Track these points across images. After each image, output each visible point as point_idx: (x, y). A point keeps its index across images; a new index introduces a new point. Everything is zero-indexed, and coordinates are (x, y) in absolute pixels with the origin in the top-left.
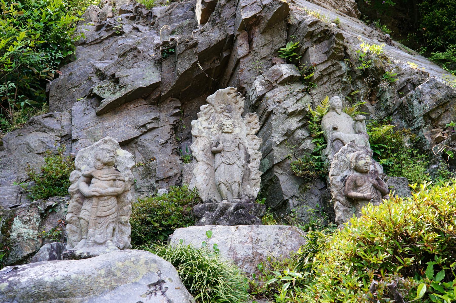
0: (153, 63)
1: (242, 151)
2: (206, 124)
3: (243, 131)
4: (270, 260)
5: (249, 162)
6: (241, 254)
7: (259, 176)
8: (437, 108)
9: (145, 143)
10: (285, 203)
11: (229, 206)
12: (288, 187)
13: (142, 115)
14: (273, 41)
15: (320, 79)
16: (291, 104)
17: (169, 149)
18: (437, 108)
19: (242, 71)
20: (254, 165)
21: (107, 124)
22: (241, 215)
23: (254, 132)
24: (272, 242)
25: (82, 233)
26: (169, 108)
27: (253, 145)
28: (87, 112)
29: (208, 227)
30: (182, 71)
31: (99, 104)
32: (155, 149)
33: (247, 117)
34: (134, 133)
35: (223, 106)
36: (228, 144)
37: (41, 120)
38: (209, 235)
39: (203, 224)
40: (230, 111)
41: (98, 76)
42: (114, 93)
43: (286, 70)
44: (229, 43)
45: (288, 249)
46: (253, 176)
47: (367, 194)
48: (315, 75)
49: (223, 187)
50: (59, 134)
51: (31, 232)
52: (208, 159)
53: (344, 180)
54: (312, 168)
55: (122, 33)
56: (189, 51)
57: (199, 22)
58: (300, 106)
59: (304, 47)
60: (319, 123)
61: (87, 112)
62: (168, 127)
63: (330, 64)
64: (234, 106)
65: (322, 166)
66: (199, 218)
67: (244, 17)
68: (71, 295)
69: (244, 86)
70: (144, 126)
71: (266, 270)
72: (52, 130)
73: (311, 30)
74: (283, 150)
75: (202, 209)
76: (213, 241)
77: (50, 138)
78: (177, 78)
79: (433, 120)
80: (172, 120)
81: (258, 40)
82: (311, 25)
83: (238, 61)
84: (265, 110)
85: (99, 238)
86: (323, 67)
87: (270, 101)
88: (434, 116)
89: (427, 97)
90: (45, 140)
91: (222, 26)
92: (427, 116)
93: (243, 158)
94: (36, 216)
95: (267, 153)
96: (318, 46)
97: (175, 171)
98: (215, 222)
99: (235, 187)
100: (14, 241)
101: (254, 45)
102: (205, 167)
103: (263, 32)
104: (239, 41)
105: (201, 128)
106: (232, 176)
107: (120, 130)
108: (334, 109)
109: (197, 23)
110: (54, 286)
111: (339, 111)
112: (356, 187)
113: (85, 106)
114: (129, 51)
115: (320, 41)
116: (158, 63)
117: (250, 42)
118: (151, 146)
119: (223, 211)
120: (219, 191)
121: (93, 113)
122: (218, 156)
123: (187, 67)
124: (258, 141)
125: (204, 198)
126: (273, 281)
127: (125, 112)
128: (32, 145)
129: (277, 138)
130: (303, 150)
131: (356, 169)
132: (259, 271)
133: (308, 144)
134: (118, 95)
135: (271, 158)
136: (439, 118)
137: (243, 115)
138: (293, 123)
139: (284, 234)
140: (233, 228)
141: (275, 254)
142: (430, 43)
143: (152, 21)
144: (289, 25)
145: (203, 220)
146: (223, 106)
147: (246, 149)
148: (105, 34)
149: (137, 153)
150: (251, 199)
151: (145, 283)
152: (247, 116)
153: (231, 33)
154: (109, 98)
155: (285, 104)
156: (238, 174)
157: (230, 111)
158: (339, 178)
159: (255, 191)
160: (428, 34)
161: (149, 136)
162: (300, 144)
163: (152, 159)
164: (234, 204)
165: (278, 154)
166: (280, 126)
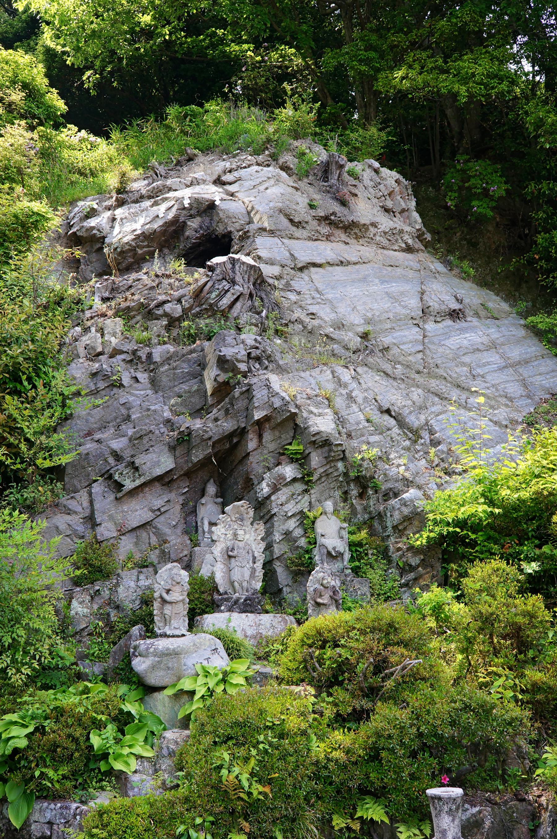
0: (167, 448)
1: (251, 555)
2: (223, 531)
3: (251, 537)
4: (267, 637)
5: (255, 563)
6: (249, 633)
7: (262, 574)
8: (404, 521)
9: (159, 526)
10: (280, 590)
11: (240, 598)
12: (283, 577)
13: (157, 499)
14: (280, 437)
15: (319, 479)
16: (291, 507)
17: (179, 531)
18: (404, 521)
19: (251, 463)
20: (259, 565)
21: (125, 508)
22: (248, 606)
23: (259, 538)
24: (268, 626)
25: (166, 621)
26: (179, 488)
27: (258, 549)
28: (105, 495)
29: (227, 614)
30: (195, 459)
31: (120, 491)
32: (167, 531)
33: (256, 526)
34: (149, 516)
35: (237, 516)
36: (241, 551)
37: (65, 503)
38: (229, 621)
39: (222, 611)
40: (242, 520)
41: (113, 456)
42: (134, 481)
43: (289, 471)
44: (241, 433)
45: (277, 631)
46: (257, 574)
47: (325, 602)
48: (314, 478)
49: (236, 584)
50: (81, 516)
51: (85, 610)
52: (225, 560)
53: (315, 590)
54: (302, 565)
55: (121, 386)
56: (204, 443)
57: (209, 393)
58: (299, 508)
59: (307, 452)
60: (313, 523)
61: (105, 495)
62: (178, 507)
63: (328, 467)
64: (245, 516)
65: (311, 563)
66: (218, 606)
67: (256, 418)
68: (181, 654)
69: (253, 477)
70: (159, 510)
71: (264, 643)
72: (76, 513)
73: (314, 439)
74: (282, 546)
75: (221, 600)
76: (232, 624)
77: (76, 521)
78: (190, 465)
79: (400, 530)
80: (181, 499)
81: (267, 436)
82: (314, 435)
83: (248, 454)
84: (269, 511)
85: (176, 625)
86: (322, 470)
87: (274, 505)
88: (401, 527)
89: (397, 513)
90: (71, 523)
91: (235, 416)
92: (395, 527)
93: (251, 562)
94: (88, 598)
95: (269, 548)
96: (319, 451)
97: (186, 552)
98: (230, 610)
99: (245, 584)
100: (73, 617)
101: (264, 440)
102: (222, 566)
103: (273, 429)
104: (251, 436)
105: (219, 533)
106: (243, 576)
107: (137, 513)
108: (326, 514)
109: (206, 392)
110: (174, 650)
111: (329, 516)
112: (321, 596)
113: (103, 488)
114: (145, 435)
115: (321, 447)
116: (172, 448)
117: (260, 437)
118: (164, 528)
119: (236, 602)
120: (233, 587)
121: (112, 497)
122: (233, 560)
123: (201, 457)
124: (263, 545)
125: (221, 590)
126: (267, 650)
127: (141, 495)
128: (60, 528)
129: (277, 537)
130: (298, 547)
131: (322, 585)
132: (259, 644)
133: (302, 542)
134: (138, 483)
135: (272, 553)
136: (405, 529)
137: (252, 524)
138: (292, 524)
139: (276, 620)
140: (244, 615)
141: (270, 633)
142: (542, 281)
143: (152, 367)
144: (296, 425)
145: (222, 608)
146: (237, 516)
147: (253, 552)
148: (102, 385)
149: (151, 534)
150: (255, 592)
151: (209, 649)
152: (255, 525)
153: (243, 425)
154: (129, 485)
155: (286, 508)
156: (247, 574)
157: (242, 520)
158: (312, 589)
159: (258, 585)
160: (542, 267)
161: (162, 518)
162: (296, 541)
163: (165, 542)
164: (244, 597)
165: (277, 550)
166: (280, 527)
